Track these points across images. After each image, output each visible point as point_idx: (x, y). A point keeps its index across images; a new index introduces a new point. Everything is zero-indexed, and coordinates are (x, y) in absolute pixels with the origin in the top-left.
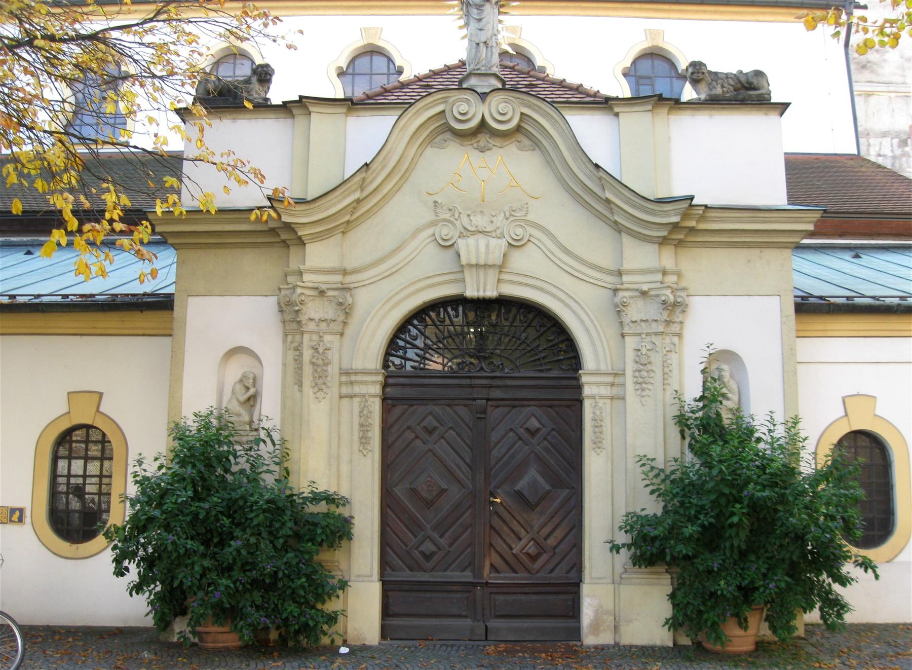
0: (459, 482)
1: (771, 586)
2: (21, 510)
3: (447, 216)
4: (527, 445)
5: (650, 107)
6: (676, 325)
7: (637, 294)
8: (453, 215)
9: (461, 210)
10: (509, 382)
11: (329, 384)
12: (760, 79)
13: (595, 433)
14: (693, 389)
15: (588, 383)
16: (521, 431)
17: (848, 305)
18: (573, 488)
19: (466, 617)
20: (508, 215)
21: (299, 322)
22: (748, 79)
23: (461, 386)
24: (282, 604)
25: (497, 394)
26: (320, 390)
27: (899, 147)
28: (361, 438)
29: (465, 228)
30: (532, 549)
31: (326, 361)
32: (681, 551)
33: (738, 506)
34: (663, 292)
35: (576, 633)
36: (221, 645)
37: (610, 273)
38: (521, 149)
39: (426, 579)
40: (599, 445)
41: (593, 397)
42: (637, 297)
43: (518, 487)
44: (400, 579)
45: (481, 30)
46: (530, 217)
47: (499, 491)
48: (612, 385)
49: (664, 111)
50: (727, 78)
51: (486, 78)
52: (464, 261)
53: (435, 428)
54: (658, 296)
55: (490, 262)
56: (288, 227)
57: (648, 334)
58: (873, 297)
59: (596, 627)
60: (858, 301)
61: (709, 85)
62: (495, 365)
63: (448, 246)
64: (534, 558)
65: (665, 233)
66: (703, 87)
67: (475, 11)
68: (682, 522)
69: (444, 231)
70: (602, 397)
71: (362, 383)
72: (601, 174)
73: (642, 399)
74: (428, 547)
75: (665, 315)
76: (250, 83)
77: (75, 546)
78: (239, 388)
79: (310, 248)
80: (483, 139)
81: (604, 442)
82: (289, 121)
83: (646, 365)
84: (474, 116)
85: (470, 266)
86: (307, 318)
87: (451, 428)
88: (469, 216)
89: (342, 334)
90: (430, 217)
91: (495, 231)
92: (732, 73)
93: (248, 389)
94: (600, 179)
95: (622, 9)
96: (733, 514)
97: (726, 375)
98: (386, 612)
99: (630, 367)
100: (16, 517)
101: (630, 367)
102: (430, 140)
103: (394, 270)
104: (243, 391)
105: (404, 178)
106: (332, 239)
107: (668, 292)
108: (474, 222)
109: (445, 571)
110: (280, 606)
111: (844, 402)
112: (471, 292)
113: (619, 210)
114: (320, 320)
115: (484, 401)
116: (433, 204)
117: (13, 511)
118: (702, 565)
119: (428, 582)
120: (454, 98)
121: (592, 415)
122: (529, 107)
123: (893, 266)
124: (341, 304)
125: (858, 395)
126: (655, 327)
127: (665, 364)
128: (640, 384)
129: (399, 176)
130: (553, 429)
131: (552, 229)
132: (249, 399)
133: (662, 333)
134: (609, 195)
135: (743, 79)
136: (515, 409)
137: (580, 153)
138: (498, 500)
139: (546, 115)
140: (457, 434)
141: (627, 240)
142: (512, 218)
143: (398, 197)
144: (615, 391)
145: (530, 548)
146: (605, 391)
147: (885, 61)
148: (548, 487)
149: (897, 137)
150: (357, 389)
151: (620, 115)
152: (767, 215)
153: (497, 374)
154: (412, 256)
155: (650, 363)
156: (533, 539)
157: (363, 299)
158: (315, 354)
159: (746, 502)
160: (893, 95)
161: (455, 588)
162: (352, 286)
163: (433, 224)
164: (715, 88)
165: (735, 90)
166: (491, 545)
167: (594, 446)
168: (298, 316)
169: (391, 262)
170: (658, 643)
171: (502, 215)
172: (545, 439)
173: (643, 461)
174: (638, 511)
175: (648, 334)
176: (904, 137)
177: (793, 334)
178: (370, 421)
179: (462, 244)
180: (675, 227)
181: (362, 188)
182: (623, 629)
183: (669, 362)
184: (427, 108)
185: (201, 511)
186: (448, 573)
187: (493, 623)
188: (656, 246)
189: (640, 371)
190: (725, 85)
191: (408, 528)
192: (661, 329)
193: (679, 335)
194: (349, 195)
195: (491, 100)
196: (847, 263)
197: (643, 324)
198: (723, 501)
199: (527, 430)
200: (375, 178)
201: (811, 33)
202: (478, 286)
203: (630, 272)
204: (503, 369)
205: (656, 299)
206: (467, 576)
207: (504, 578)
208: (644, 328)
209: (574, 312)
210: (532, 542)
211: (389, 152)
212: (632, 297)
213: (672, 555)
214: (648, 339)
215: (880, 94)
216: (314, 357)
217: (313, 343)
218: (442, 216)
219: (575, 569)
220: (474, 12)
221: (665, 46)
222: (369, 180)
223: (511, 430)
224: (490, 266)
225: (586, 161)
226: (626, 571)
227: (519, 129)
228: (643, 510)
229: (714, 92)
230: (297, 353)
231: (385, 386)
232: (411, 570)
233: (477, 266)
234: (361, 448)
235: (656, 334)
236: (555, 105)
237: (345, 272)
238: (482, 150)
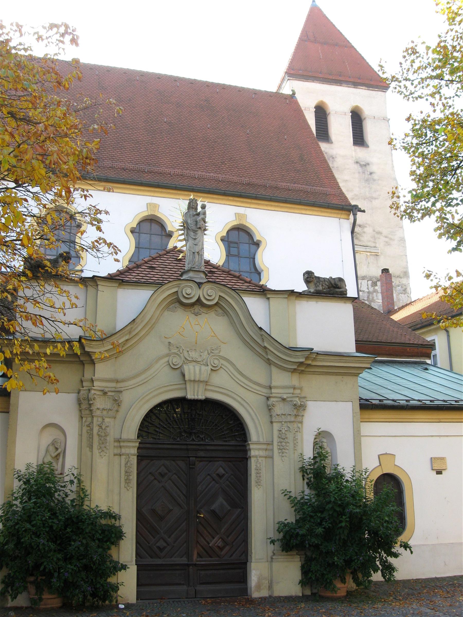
0: (180, 505)
1: (361, 559)
3: (176, 351)
4: (217, 483)
5: (287, 296)
6: (300, 417)
7: (280, 400)
8: (179, 351)
9: (184, 348)
10: (208, 448)
11: (108, 447)
12: (342, 283)
13: (257, 477)
14: (309, 453)
15: (253, 449)
16: (214, 475)
17: (407, 405)
18: (243, 508)
19: (183, 584)
20: (209, 352)
21: (91, 411)
22: (335, 282)
23: (181, 449)
24: (95, 579)
25: (201, 454)
26: (103, 451)
27: (372, 286)
28: (126, 480)
29: (186, 359)
30: (220, 543)
31: (107, 434)
32: (314, 542)
33: (344, 517)
34: (294, 399)
35: (245, 591)
36: (49, 606)
37: (265, 387)
38: (217, 315)
39: (160, 563)
40: (259, 483)
41: (256, 457)
42: (280, 401)
43: (213, 508)
44: (145, 563)
45: (196, 245)
46: (221, 354)
47: (202, 510)
48: (266, 450)
49: (293, 298)
50: (325, 281)
51: (199, 273)
52: (187, 378)
54: (291, 401)
55: (202, 380)
57: (285, 422)
58: (393, 400)
59: (259, 587)
60: (385, 402)
61: (315, 284)
62: (200, 438)
64: (221, 549)
65: (295, 367)
66: (312, 285)
67: (192, 233)
68: (313, 526)
69: (175, 360)
70: (260, 457)
71: (127, 447)
73: (283, 458)
74: (161, 544)
75: (295, 412)
76: (58, 262)
78: (52, 449)
79: (98, 366)
80: (197, 308)
81: (262, 482)
83: (284, 439)
84: (194, 296)
85: (190, 381)
86: (96, 408)
87: (175, 473)
88: (188, 351)
89: (115, 418)
90: (166, 351)
91: (203, 361)
92: (326, 278)
94: (261, 335)
95: (222, 199)
96: (341, 522)
97: (325, 445)
98: (139, 584)
99: (276, 440)
101: (276, 440)
102: (167, 307)
103: (145, 381)
104: (54, 450)
105: (152, 328)
106: (110, 361)
107: (297, 399)
108: (191, 355)
109: (171, 557)
110: (94, 580)
111: (379, 458)
112: (190, 396)
113: (271, 353)
114: (103, 409)
115: (194, 458)
116: (168, 344)
118: (325, 549)
119: (162, 564)
120: (184, 285)
121: (255, 467)
122: (222, 292)
125: (386, 454)
126: (289, 418)
127: (295, 439)
128: (282, 449)
129: (150, 326)
130: (232, 475)
131: (233, 360)
132: (56, 456)
133: (292, 422)
134: (266, 345)
135: (333, 282)
136: (210, 463)
137: (251, 320)
138: (202, 516)
139: (233, 298)
140: (178, 477)
141: (274, 369)
142: (212, 354)
144: (267, 453)
145: (219, 543)
146: (262, 453)
147: (364, 232)
148: (229, 508)
149: (370, 280)
150: (123, 451)
151: (271, 299)
152: (347, 359)
153: (201, 443)
154: (156, 373)
155: (286, 438)
156: (221, 538)
157: (126, 398)
158: (100, 430)
159: (348, 515)
160: (369, 254)
161: (178, 567)
162: (122, 389)
163: (168, 355)
164: (318, 286)
165: (329, 288)
166: (198, 542)
167: (256, 484)
168: (90, 407)
169: (143, 377)
170: (294, 594)
171: (206, 352)
172: (227, 480)
173: (286, 493)
174: (283, 520)
175: (285, 422)
176: (375, 280)
177: (359, 421)
178: (131, 469)
179: (186, 369)
180: (301, 364)
181: (130, 333)
183: (296, 437)
184: (168, 289)
185: (54, 525)
186: (173, 559)
187: (200, 588)
188: (290, 373)
189: (281, 442)
190: (324, 285)
191: (149, 532)
192: (293, 419)
193: (301, 422)
194: (123, 337)
195: (204, 288)
197: (283, 416)
198: (335, 515)
199: (218, 475)
200: (137, 327)
201: (355, 104)
202: (194, 392)
203: (276, 387)
204: (205, 440)
205: (291, 403)
206: (184, 560)
207: (205, 561)
208: (283, 418)
209: (245, 408)
210: (220, 540)
211: (146, 313)
212: (277, 401)
213: (309, 544)
214: (286, 425)
215: (361, 252)
216: (99, 431)
217: (99, 423)
218: (173, 351)
219: (244, 555)
220: (192, 234)
221: (247, 225)
222: (134, 328)
223: (209, 475)
224: (201, 381)
225: (254, 325)
226: (274, 554)
227: (217, 304)
228: (286, 520)
229: (318, 288)
230: (89, 428)
231: (139, 448)
232: (151, 557)
233: (194, 381)
234: (126, 486)
235: (290, 422)
236: (237, 291)
237: (117, 381)
238: (196, 314)
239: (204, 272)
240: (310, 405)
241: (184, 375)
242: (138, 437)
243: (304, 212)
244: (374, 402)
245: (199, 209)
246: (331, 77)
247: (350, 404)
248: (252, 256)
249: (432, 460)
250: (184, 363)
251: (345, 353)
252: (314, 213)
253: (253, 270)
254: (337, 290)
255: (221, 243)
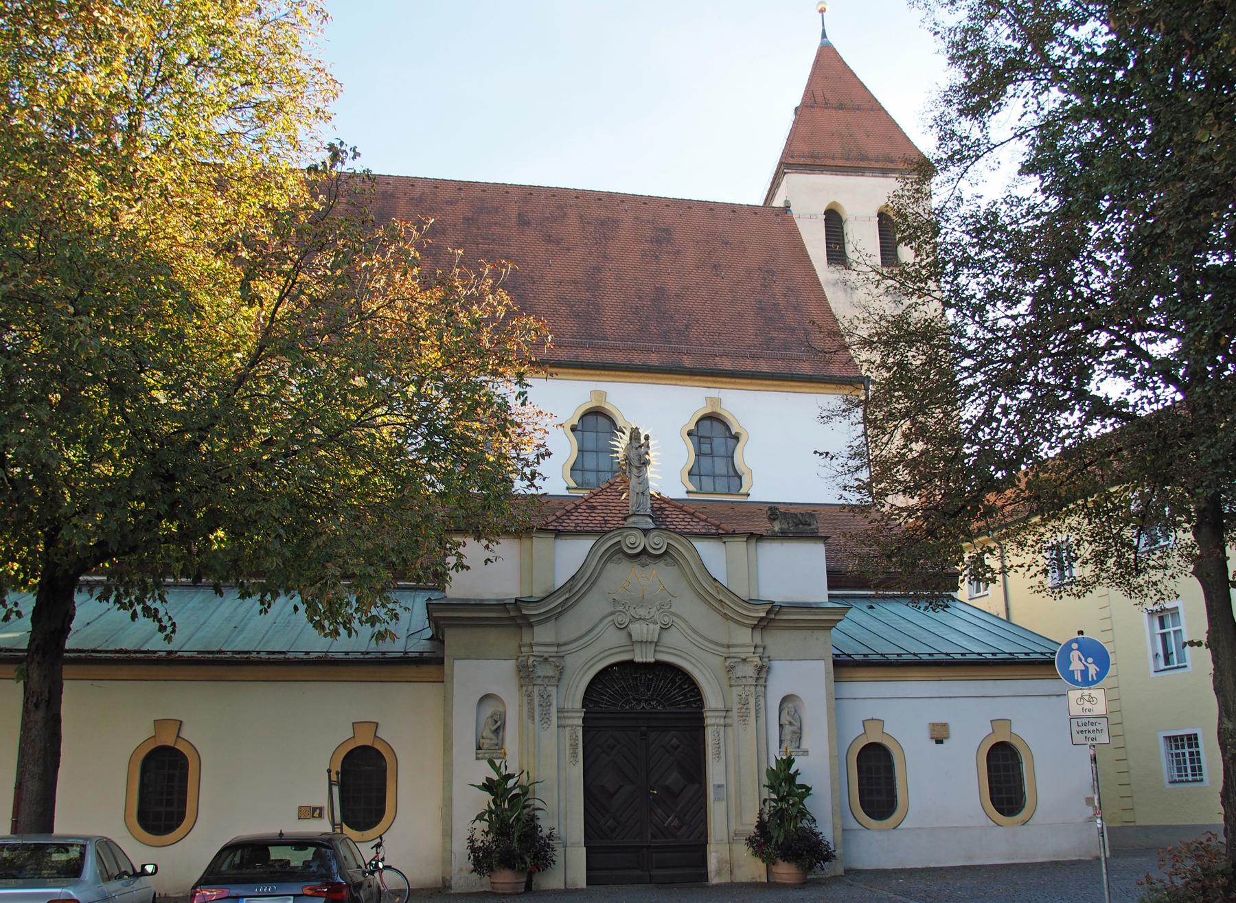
2: (321, 809)
3: (621, 608)
17: (897, 661)
35: (705, 876)
41: (713, 725)
43: (667, 783)
46: (672, 610)
52: (634, 639)
53: (678, 746)
56: (526, 617)
59: (719, 873)
63: (621, 628)
72: (717, 584)
77: (361, 833)
80: (644, 559)
82: (517, 541)
90: (610, 609)
93: (496, 722)
100: (316, 814)
105: (594, 583)
112: (638, 659)
117: (314, 809)
123: (897, 618)
124: (558, 666)
139: (683, 545)
141: (733, 625)
143: (589, 595)
157: (571, 662)
169: (586, 639)
180: (762, 619)
181: (570, 590)
182: (736, 871)
187: (654, 872)
196: (865, 615)
218: (618, 609)
221: (722, 412)
231: (584, 719)
233: (641, 642)
237: (559, 645)
239: (649, 516)
240: (774, 663)
241: (630, 635)
242: (583, 707)
243: (798, 390)
244: (856, 658)
245: (643, 441)
246: (848, 164)
247: (822, 662)
248: (730, 454)
249: (933, 726)
250: (630, 622)
251: (815, 603)
252: (812, 390)
253: (732, 473)
254: (806, 527)
255: (688, 439)
